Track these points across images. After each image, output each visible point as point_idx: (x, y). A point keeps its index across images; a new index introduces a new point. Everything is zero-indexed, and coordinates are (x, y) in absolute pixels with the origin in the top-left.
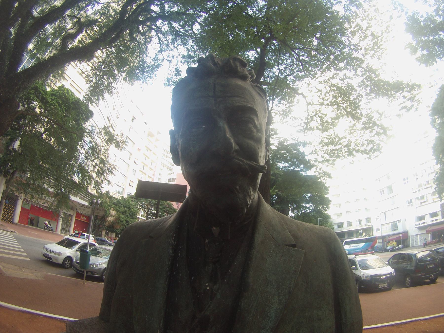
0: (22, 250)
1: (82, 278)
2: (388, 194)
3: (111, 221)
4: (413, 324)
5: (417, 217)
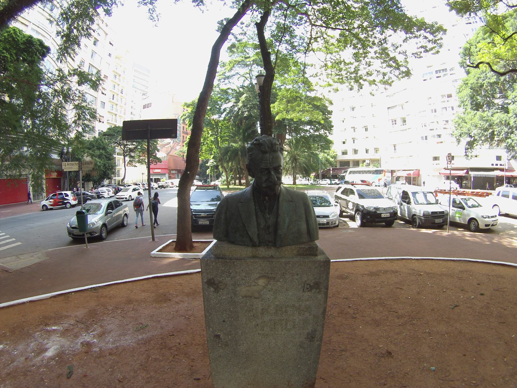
0: (8, 236)
1: (85, 243)
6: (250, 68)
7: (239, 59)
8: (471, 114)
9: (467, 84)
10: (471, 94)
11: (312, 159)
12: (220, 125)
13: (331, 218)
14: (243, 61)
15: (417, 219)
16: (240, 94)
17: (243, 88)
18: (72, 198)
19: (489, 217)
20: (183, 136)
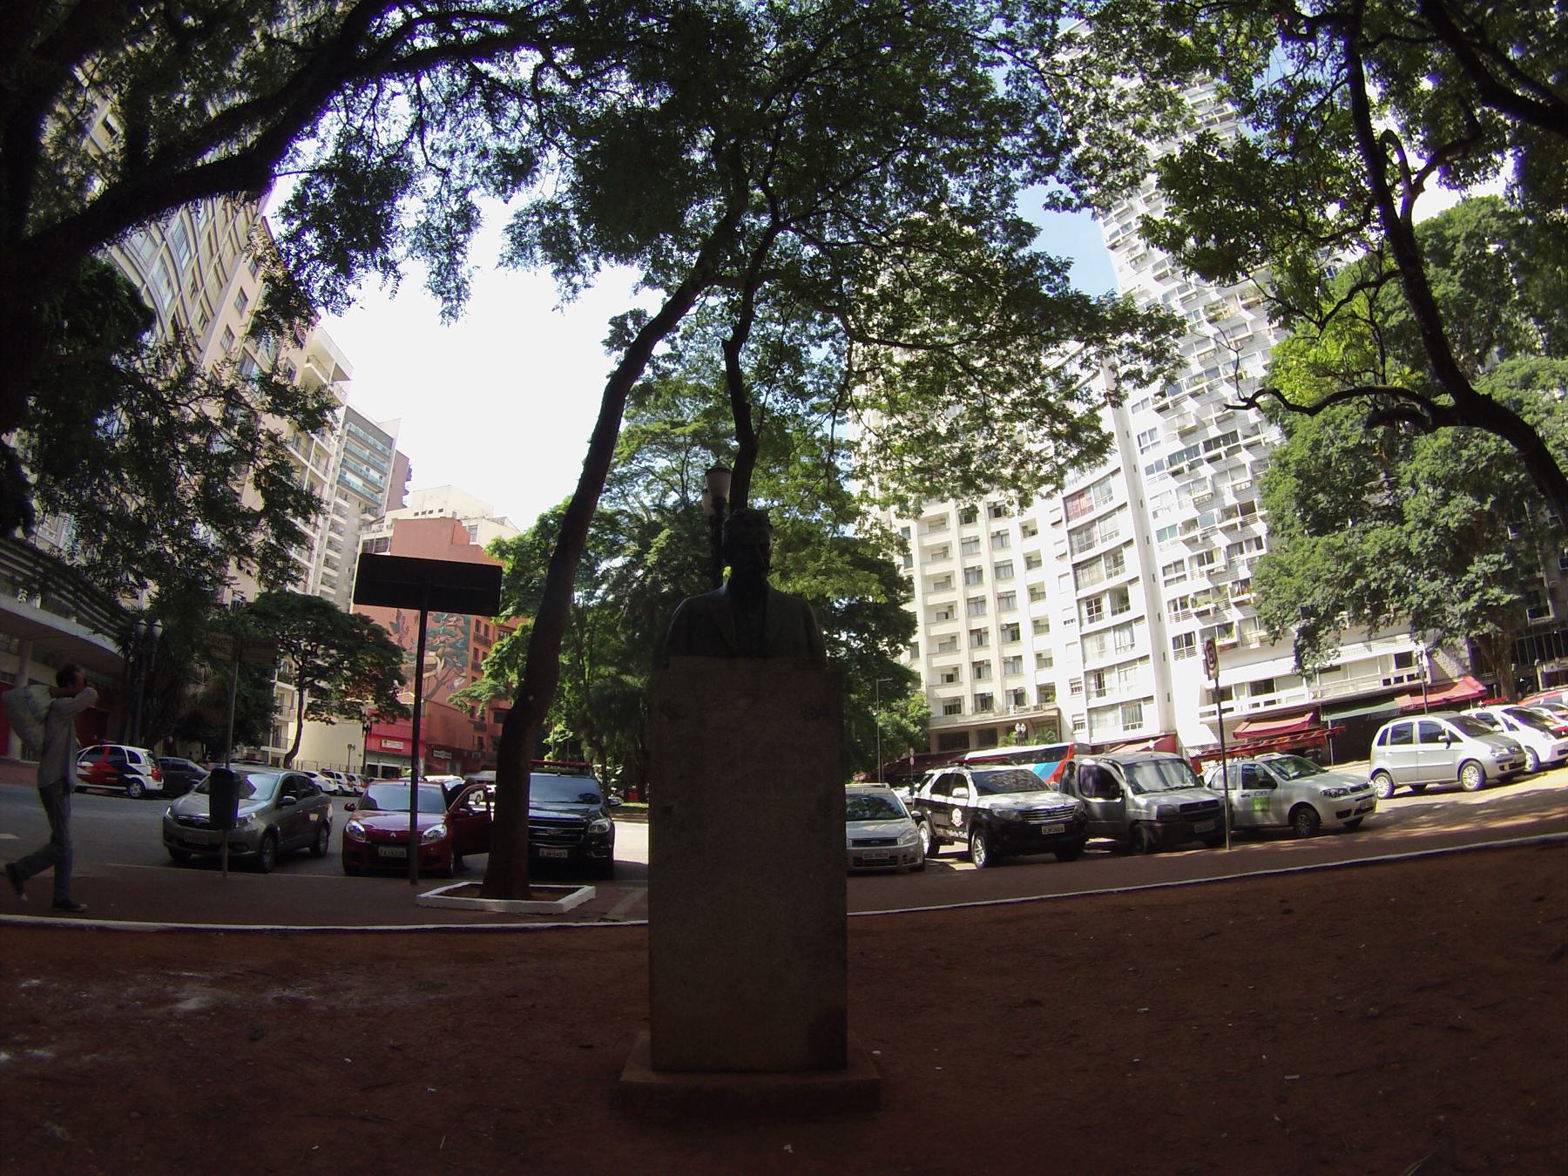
2: (1114, 613)
3: (199, 697)
4: (512, 938)
5: (1207, 691)
6: (683, 455)
7: (656, 427)
8: (1305, 547)
9: (1287, 464)
10: (1297, 490)
11: (853, 727)
12: (589, 618)
13: (901, 844)
14: (665, 432)
15: (1144, 831)
16: (654, 529)
17: (662, 514)
18: (149, 770)
19: (1345, 792)
20: (476, 650)
